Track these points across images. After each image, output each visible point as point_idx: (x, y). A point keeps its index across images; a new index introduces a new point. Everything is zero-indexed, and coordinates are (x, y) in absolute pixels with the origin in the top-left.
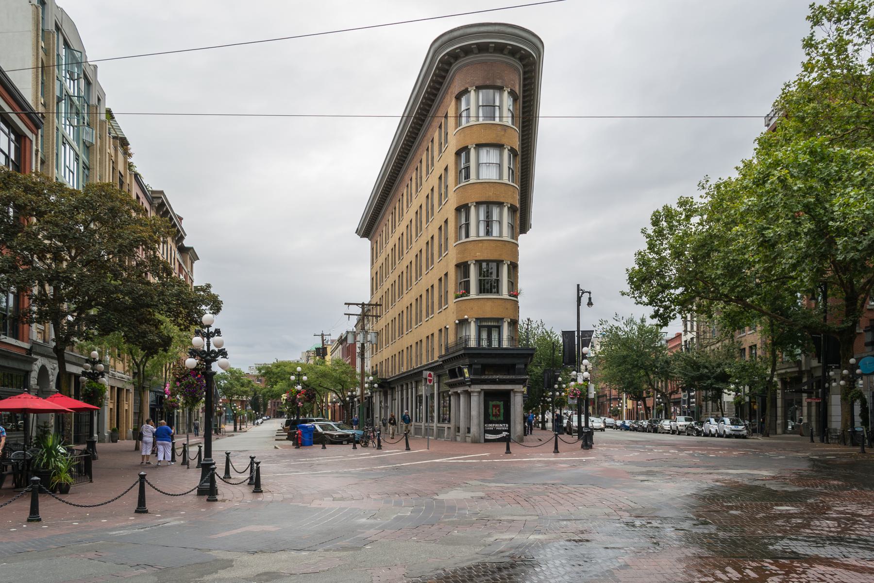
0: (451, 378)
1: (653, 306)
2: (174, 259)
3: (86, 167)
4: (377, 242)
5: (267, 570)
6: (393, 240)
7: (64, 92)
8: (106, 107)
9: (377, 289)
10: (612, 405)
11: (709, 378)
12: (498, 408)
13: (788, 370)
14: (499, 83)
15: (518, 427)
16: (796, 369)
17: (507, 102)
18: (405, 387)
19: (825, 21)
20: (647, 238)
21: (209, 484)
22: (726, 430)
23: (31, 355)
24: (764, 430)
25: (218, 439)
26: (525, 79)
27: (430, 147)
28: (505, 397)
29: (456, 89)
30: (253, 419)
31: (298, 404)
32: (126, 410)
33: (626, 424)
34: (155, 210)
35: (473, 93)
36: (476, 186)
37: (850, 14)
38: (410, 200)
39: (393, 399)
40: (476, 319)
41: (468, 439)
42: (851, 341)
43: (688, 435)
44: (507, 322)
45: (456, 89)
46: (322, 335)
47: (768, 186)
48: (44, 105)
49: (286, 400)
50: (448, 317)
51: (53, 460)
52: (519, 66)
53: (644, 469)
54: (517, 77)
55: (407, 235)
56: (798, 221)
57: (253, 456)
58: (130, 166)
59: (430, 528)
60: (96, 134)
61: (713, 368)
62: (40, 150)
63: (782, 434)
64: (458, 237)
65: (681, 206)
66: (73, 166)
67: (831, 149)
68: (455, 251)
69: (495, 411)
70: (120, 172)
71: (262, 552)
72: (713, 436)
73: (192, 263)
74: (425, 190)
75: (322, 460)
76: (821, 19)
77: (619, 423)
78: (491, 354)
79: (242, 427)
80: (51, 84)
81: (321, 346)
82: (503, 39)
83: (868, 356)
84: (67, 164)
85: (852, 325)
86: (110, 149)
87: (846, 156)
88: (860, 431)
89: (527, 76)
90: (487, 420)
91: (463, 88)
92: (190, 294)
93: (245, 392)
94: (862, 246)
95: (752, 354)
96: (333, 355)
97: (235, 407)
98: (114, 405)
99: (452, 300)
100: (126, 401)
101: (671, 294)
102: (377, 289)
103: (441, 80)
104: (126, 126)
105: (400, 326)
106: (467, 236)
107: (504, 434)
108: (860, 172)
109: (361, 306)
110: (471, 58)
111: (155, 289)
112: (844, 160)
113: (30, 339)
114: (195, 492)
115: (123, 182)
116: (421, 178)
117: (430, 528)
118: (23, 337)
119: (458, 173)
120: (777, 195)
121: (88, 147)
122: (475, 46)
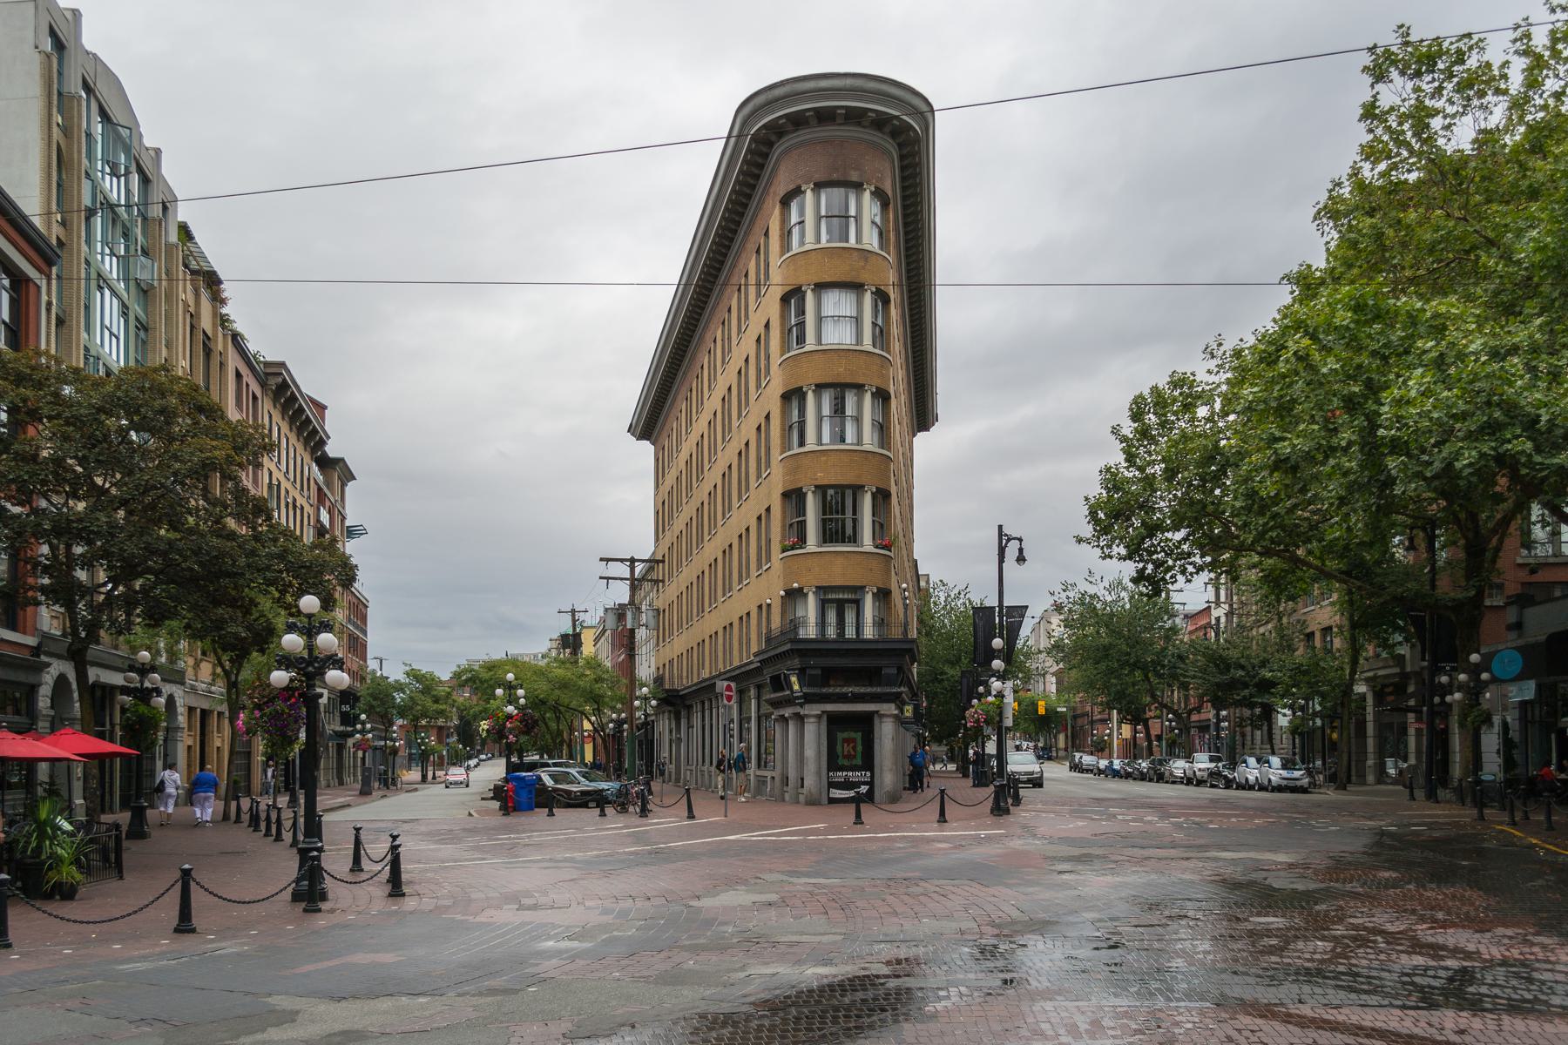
0: (775, 692)
1: (1135, 561)
2: (309, 479)
3: (142, 327)
4: (663, 449)
5: (346, 1027)
6: (688, 447)
7: (99, 198)
8: (179, 220)
9: (664, 531)
10: (1095, 732)
11: (1246, 686)
12: (851, 745)
13: (1381, 673)
14: (854, 176)
15: (888, 776)
16: (1396, 670)
17: (870, 208)
18: (707, 705)
19: (1394, 74)
20: (1122, 442)
21: (306, 883)
22: (1272, 778)
23: (38, 656)
24: (1339, 780)
25: (384, 797)
26: (902, 169)
28: (865, 723)
30: (457, 759)
31: (508, 738)
32: (218, 748)
33: (1115, 767)
34: (272, 396)
35: (809, 194)
36: (816, 357)
37: (1436, 63)
38: (713, 378)
39: (690, 726)
41: (802, 798)
42: (1473, 624)
43: (1213, 786)
44: (870, 593)
45: (781, 187)
46: (573, 612)
47: (1282, 367)
48: (63, 223)
49: (488, 731)
50: (767, 587)
51: (47, 843)
52: (890, 146)
53: (1076, 852)
54: (887, 165)
55: (709, 437)
56: (1331, 427)
57: (395, 833)
58: (224, 321)
59: (653, 956)
60: (160, 268)
61: (1253, 668)
62: (54, 302)
63: (1376, 784)
64: (786, 446)
65: (1175, 387)
66: (118, 325)
67: (1393, 301)
69: (847, 749)
70: (204, 332)
71: (354, 997)
72: (1251, 788)
73: (343, 485)
75: (536, 837)
76: (1387, 71)
77: (1103, 763)
78: (820, 650)
79: (438, 773)
80: (75, 187)
81: (570, 632)
82: (861, 101)
83: (1507, 648)
84: (107, 322)
85: (1475, 596)
86: (185, 293)
87: (1415, 314)
88: (1489, 782)
89: (906, 162)
90: (833, 765)
91: (792, 187)
92: (301, 554)
93: (441, 713)
94: (1431, 471)
95: (1325, 642)
96: (598, 646)
97: (423, 738)
98: (195, 739)
100: (219, 732)
101: (1167, 540)
102: (664, 531)
103: (756, 171)
104: (214, 248)
105: (700, 596)
106: (802, 443)
107: (864, 789)
108: (1433, 343)
109: (628, 563)
110: (804, 135)
111: (239, 547)
112: (1413, 319)
113: (37, 629)
114: (287, 895)
115: (210, 350)
116: (730, 338)
117: (653, 956)
118: (25, 627)
119: (786, 332)
120: (1297, 382)
121: (145, 292)
122: (811, 113)
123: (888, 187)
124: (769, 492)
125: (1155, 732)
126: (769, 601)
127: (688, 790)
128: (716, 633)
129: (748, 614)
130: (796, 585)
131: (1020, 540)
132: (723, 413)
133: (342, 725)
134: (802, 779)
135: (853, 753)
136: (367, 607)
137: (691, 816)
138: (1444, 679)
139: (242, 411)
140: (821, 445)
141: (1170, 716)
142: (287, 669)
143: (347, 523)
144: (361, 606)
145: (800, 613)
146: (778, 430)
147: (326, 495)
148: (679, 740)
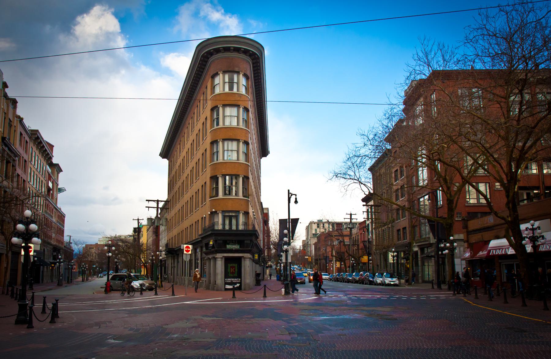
6: (179, 161)
12: (234, 269)
14: (237, 69)
28: (239, 261)
29: (211, 72)
38: (188, 137)
39: (178, 262)
40: (222, 211)
46: (138, 220)
50: (205, 211)
54: (249, 67)
69: (232, 270)
73: (58, 173)
81: (137, 226)
90: (226, 276)
91: (215, 72)
97: (83, 265)
99: (208, 200)
105: (182, 215)
107: (238, 285)
109: (156, 202)
115: (11, 125)
116: (194, 123)
123: (248, 73)
125: (348, 265)
126: (205, 216)
127: (173, 285)
129: (198, 221)
130: (214, 210)
131: (296, 195)
133: (53, 260)
134: (215, 281)
135: (234, 272)
136: (65, 217)
137: (173, 294)
138: (442, 245)
139: (22, 147)
140: (224, 160)
141: (353, 259)
142: (18, 238)
143: (59, 187)
144: (62, 217)
145: (216, 220)
147: (51, 176)
148: (174, 267)
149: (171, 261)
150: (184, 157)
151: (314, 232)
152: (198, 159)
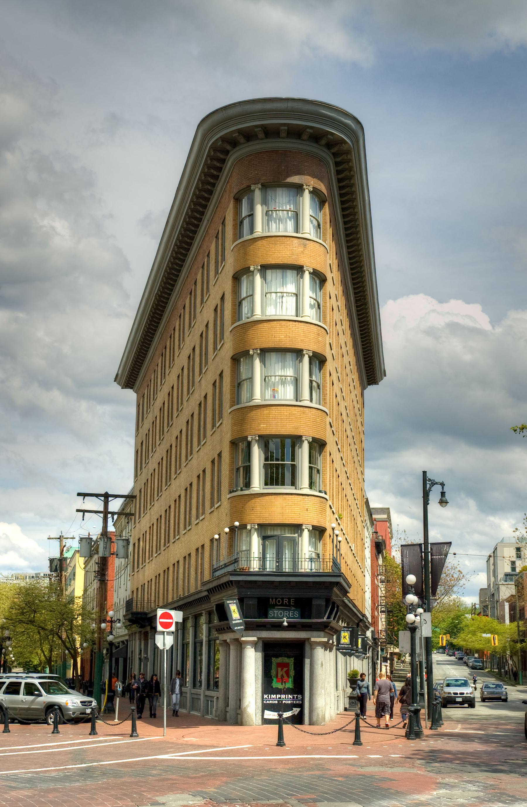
6: (162, 396)
12: (285, 669)
27: (206, 263)
38: (182, 339)
55: (178, 389)
68: (230, 421)
74: (199, 327)
81: (57, 555)
82: (300, 119)
91: (244, 186)
99: (225, 496)
107: (296, 711)
109: (103, 498)
122: (259, 129)
123: (322, 187)
124: (221, 439)
126: (217, 537)
128: (178, 562)
131: (443, 485)
132: (189, 369)
140: (265, 400)
146: (229, 386)
149: (140, 645)
150: (173, 388)
151: (508, 570)
152: (203, 395)
